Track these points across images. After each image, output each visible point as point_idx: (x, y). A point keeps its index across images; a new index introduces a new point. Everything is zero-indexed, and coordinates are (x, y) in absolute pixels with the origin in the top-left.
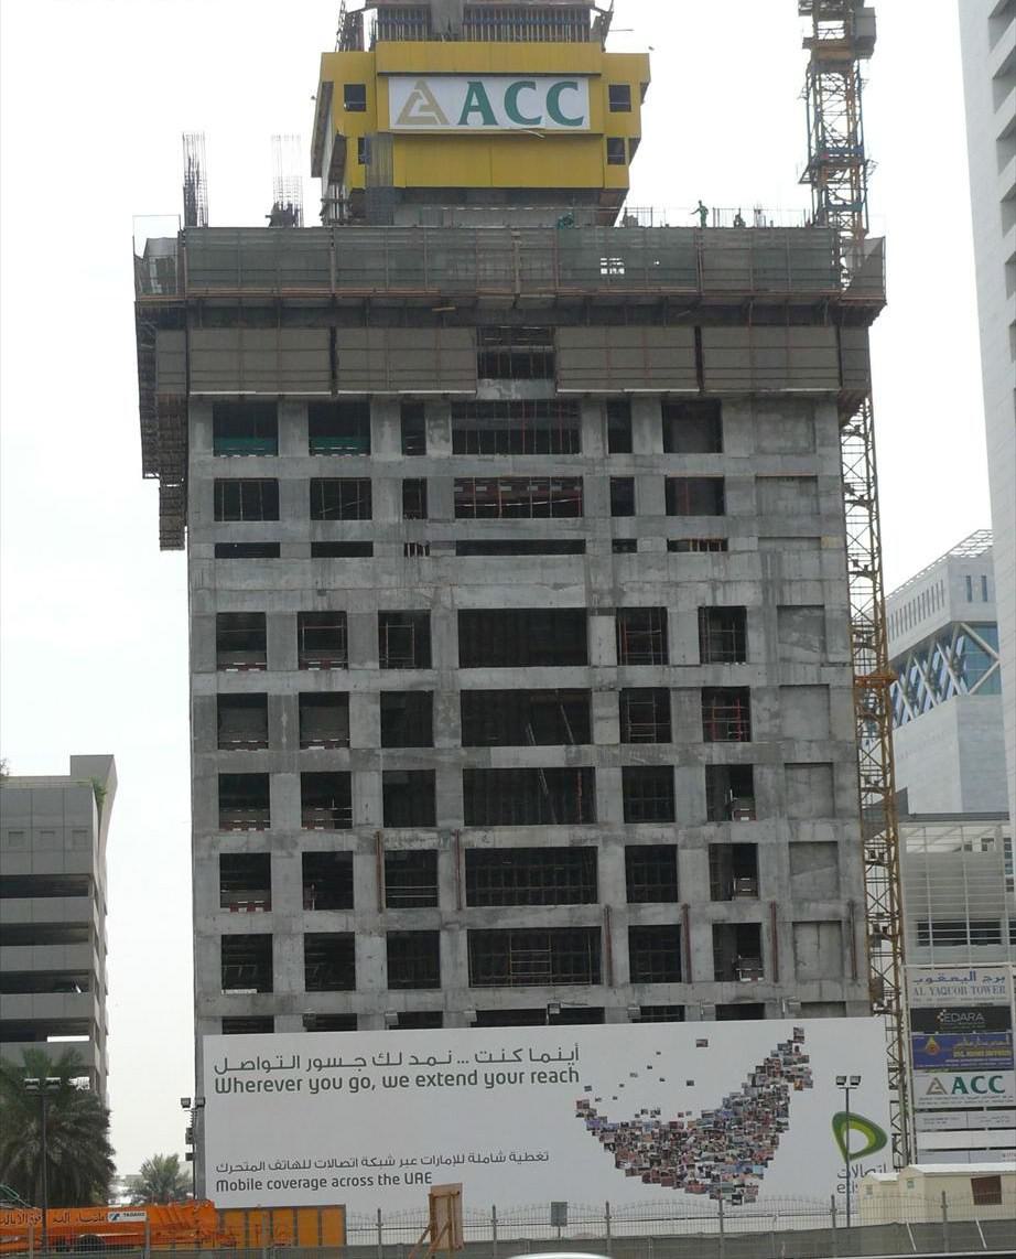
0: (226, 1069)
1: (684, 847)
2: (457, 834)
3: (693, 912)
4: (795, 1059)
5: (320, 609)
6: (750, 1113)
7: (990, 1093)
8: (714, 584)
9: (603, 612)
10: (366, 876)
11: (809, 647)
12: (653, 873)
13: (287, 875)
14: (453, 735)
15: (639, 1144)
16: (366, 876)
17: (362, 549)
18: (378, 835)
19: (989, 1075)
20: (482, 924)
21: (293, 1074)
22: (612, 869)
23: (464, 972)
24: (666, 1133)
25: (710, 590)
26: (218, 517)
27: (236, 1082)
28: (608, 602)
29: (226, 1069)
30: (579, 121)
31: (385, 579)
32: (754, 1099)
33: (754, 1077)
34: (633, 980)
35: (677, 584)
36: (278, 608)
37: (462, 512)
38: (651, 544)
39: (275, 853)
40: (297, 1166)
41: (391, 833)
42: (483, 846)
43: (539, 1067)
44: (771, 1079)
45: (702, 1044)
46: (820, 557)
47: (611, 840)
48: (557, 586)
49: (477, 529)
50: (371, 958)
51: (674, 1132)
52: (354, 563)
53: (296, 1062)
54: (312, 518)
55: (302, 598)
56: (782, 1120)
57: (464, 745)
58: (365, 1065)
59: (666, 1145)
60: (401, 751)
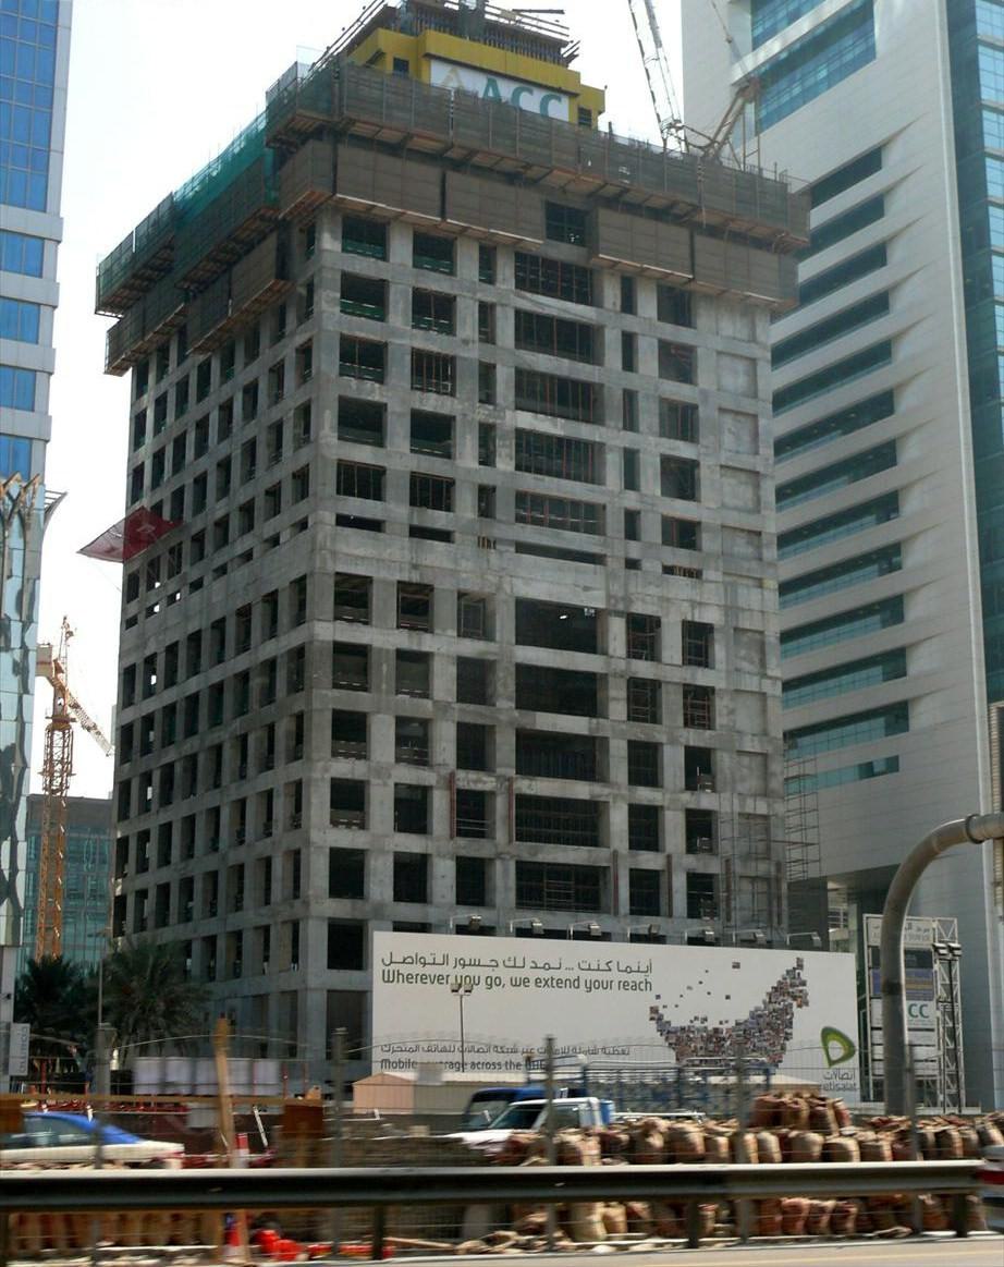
0: (391, 962)
1: (669, 809)
2: (510, 780)
3: (674, 860)
4: (797, 982)
5: (414, 581)
6: (768, 1024)
7: (920, 1017)
8: (694, 604)
9: (619, 614)
10: (440, 807)
11: (752, 663)
12: (645, 825)
13: (381, 805)
14: (509, 699)
15: (693, 1045)
16: (440, 807)
17: (445, 536)
18: (452, 775)
19: (919, 1003)
20: (526, 857)
23: (512, 896)
24: (711, 1036)
25: (690, 609)
26: (338, 492)
27: (399, 974)
28: (621, 607)
29: (391, 962)
32: (770, 1013)
33: (770, 995)
34: (632, 912)
35: (668, 600)
38: (652, 566)
39: (374, 781)
40: (444, 1050)
41: (461, 774)
42: (528, 792)
43: (625, 977)
44: (781, 998)
45: (736, 966)
46: (762, 594)
47: (617, 799)
48: (586, 589)
49: (530, 534)
50: (443, 877)
52: (440, 546)
53: (446, 959)
54: (413, 503)
55: (401, 570)
56: (789, 1031)
57: (517, 708)
58: (497, 966)
60: (472, 707)
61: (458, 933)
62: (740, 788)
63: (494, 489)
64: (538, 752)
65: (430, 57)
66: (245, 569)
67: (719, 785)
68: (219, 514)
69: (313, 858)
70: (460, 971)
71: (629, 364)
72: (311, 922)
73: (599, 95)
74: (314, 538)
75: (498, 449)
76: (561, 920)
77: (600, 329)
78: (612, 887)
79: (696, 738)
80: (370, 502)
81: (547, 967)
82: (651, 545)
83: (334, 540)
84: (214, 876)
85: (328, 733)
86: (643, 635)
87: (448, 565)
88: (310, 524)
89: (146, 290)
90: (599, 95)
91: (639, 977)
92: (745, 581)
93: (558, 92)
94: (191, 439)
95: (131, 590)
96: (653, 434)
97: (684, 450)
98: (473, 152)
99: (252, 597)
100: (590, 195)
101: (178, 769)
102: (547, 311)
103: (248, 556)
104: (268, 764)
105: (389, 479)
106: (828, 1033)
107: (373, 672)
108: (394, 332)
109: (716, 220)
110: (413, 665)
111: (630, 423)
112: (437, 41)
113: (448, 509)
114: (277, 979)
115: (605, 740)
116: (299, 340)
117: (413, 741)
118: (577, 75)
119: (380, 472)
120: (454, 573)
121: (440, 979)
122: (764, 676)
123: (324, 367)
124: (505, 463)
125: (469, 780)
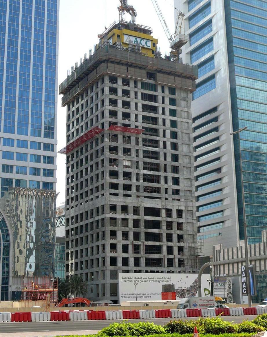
2: (144, 242)
3: (176, 256)
8: (179, 206)
9: (164, 209)
12: (170, 250)
13: (119, 248)
16: (131, 248)
17: (130, 196)
18: (133, 242)
20: (147, 257)
21: (132, 280)
22: (165, 249)
23: (145, 264)
28: (164, 207)
30: (150, 47)
31: (134, 201)
34: (168, 267)
35: (174, 205)
36: (119, 204)
37: (145, 191)
39: (118, 244)
40: (132, 294)
41: (134, 241)
45: (187, 277)
47: (164, 244)
48: (158, 204)
49: (147, 194)
50: (131, 261)
51: (183, 290)
53: (132, 277)
54: (124, 190)
59: (183, 292)
61: (135, 272)
62: (188, 242)
63: (139, 186)
64: (149, 237)
65: (124, 34)
66: (92, 202)
67: (184, 241)
68: (86, 190)
69: (107, 259)
70: (135, 280)
71: (165, 159)
72: (107, 271)
73: (157, 40)
74: (105, 198)
75: (140, 178)
76: (154, 269)
77: (159, 152)
78: (164, 261)
79: (179, 232)
80: (116, 190)
81: (151, 278)
82: (170, 195)
83: (109, 198)
84: (87, 261)
85: (109, 235)
86: (169, 212)
87: (131, 201)
88: (105, 195)
89: (69, 90)
90: (157, 40)
91: (168, 280)
92: (189, 201)
93: (148, 40)
94: (79, 174)
95: (68, 158)
96: (170, 173)
97: (176, 175)
98: (132, 63)
99: (94, 208)
100: (155, 70)
101: (79, 240)
102: (149, 150)
103: (92, 199)
104: (97, 240)
105: (119, 185)
106: (205, 289)
107: (117, 223)
108: (119, 157)
109: (179, 74)
110: (125, 220)
111: (166, 171)
112: (125, 31)
113: (131, 190)
114: (100, 256)
115: (162, 233)
116: (101, 158)
117: (125, 235)
118: (152, 37)
119: (118, 184)
120: (132, 203)
121: (131, 281)
122: (193, 219)
123: (106, 165)
124: (141, 181)
125: (136, 243)
